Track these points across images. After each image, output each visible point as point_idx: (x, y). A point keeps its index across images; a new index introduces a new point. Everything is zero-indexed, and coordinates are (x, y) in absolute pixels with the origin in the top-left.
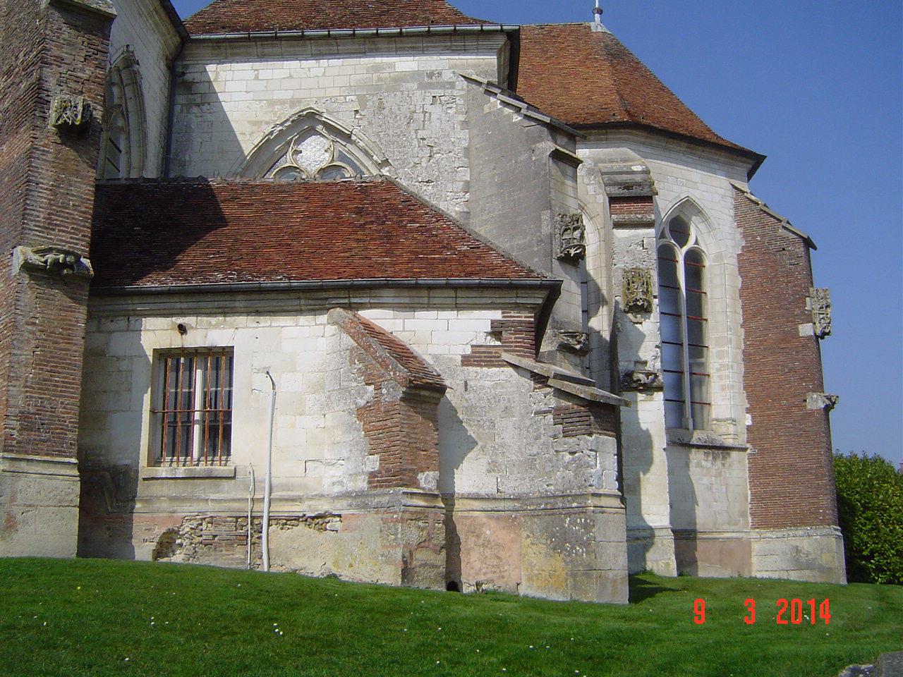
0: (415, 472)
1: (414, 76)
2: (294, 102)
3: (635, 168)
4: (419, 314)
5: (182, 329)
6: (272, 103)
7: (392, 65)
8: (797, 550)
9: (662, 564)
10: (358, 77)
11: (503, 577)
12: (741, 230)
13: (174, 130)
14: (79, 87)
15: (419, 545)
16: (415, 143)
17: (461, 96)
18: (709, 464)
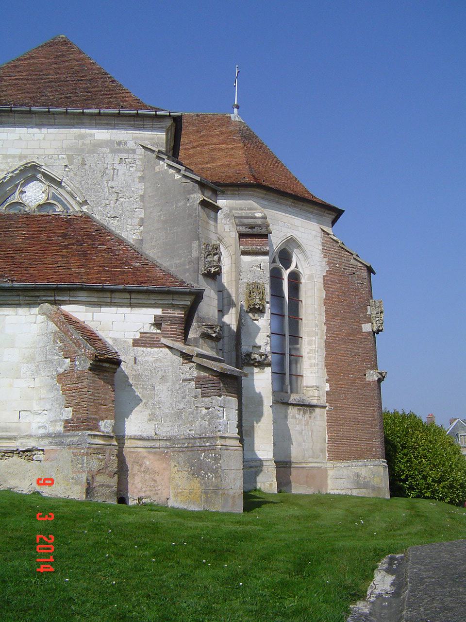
1: (108, 143)
2: (21, 157)
3: (257, 215)
4: (103, 309)
7: (92, 135)
8: (358, 475)
11: (157, 494)
12: (326, 259)
15: (99, 472)
16: (106, 190)
18: (301, 417)
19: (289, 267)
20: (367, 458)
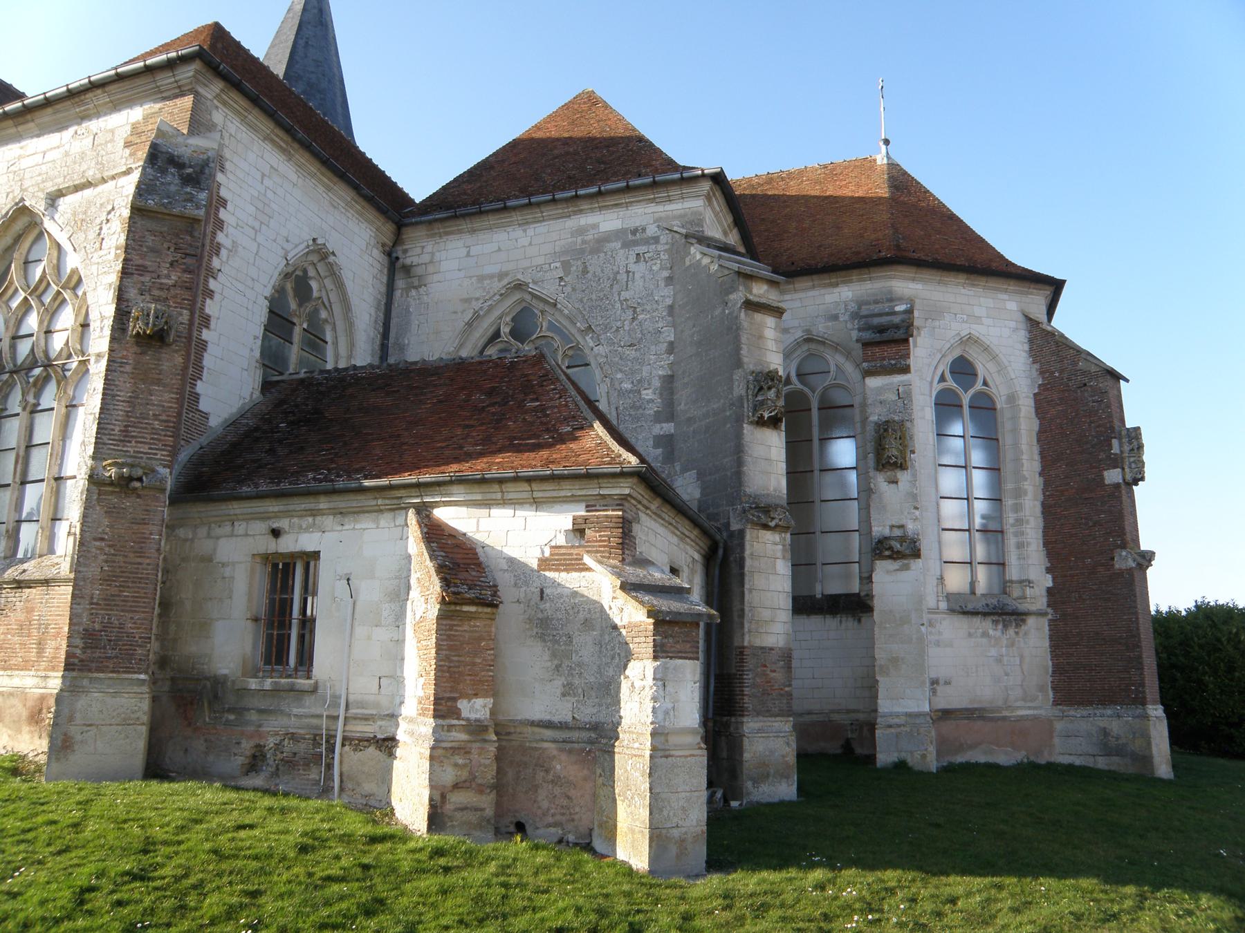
0: (455, 700)
1: (618, 234)
2: (502, 276)
3: (898, 309)
4: (496, 512)
5: (276, 533)
6: (481, 278)
7: (595, 226)
8: (1105, 732)
9: (917, 755)
10: (563, 242)
11: (573, 820)
12: (1037, 366)
13: (393, 314)
14: (163, 294)
15: (456, 786)
16: (618, 305)
17: (665, 251)
18: (998, 633)
19: (972, 386)
20: (1121, 704)
